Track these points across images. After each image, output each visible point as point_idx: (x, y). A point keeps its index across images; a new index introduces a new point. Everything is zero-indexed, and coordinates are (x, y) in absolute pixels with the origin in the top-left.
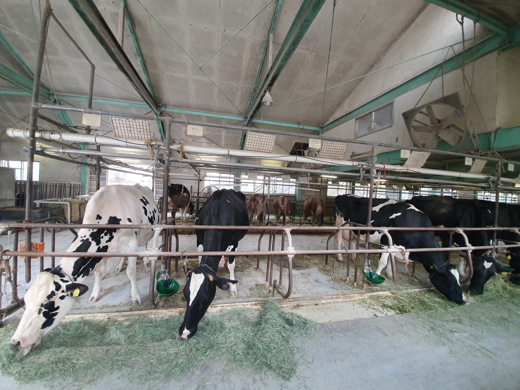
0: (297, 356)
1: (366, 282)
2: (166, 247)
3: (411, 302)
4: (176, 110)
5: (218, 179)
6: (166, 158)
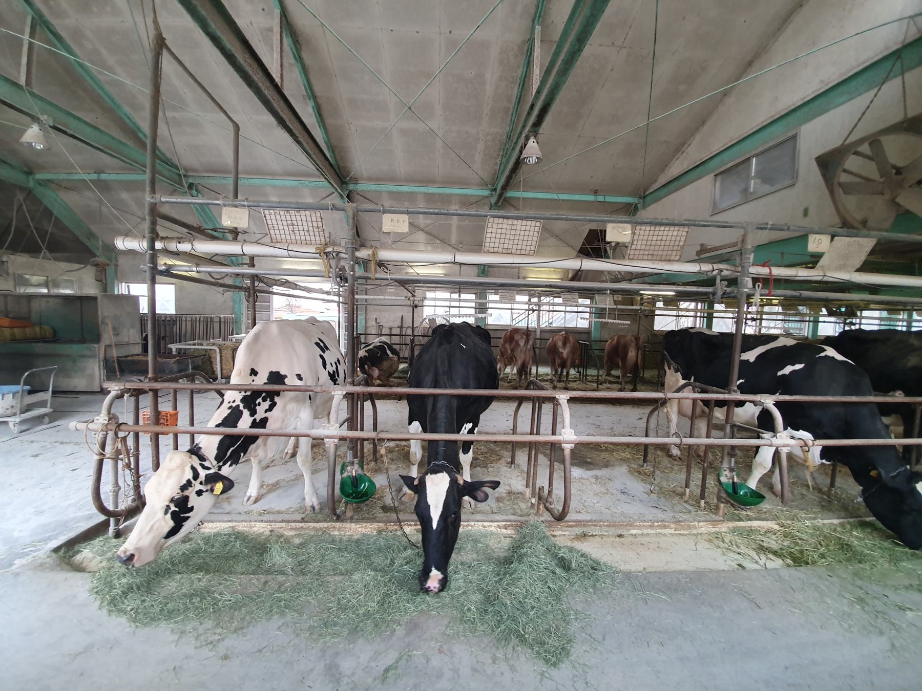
0: (574, 627)
1: (723, 500)
2: (353, 422)
3: (821, 545)
4: (373, 187)
5: (447, 304)
6: (349, 274)
